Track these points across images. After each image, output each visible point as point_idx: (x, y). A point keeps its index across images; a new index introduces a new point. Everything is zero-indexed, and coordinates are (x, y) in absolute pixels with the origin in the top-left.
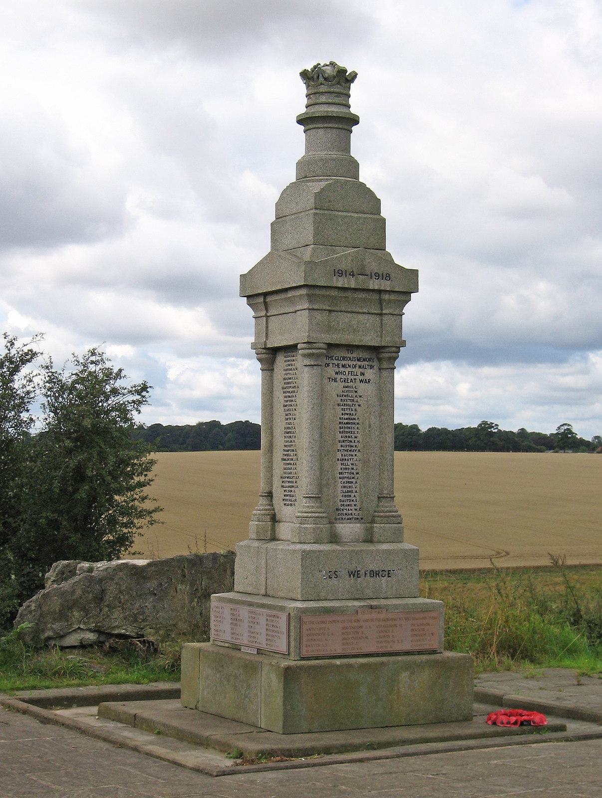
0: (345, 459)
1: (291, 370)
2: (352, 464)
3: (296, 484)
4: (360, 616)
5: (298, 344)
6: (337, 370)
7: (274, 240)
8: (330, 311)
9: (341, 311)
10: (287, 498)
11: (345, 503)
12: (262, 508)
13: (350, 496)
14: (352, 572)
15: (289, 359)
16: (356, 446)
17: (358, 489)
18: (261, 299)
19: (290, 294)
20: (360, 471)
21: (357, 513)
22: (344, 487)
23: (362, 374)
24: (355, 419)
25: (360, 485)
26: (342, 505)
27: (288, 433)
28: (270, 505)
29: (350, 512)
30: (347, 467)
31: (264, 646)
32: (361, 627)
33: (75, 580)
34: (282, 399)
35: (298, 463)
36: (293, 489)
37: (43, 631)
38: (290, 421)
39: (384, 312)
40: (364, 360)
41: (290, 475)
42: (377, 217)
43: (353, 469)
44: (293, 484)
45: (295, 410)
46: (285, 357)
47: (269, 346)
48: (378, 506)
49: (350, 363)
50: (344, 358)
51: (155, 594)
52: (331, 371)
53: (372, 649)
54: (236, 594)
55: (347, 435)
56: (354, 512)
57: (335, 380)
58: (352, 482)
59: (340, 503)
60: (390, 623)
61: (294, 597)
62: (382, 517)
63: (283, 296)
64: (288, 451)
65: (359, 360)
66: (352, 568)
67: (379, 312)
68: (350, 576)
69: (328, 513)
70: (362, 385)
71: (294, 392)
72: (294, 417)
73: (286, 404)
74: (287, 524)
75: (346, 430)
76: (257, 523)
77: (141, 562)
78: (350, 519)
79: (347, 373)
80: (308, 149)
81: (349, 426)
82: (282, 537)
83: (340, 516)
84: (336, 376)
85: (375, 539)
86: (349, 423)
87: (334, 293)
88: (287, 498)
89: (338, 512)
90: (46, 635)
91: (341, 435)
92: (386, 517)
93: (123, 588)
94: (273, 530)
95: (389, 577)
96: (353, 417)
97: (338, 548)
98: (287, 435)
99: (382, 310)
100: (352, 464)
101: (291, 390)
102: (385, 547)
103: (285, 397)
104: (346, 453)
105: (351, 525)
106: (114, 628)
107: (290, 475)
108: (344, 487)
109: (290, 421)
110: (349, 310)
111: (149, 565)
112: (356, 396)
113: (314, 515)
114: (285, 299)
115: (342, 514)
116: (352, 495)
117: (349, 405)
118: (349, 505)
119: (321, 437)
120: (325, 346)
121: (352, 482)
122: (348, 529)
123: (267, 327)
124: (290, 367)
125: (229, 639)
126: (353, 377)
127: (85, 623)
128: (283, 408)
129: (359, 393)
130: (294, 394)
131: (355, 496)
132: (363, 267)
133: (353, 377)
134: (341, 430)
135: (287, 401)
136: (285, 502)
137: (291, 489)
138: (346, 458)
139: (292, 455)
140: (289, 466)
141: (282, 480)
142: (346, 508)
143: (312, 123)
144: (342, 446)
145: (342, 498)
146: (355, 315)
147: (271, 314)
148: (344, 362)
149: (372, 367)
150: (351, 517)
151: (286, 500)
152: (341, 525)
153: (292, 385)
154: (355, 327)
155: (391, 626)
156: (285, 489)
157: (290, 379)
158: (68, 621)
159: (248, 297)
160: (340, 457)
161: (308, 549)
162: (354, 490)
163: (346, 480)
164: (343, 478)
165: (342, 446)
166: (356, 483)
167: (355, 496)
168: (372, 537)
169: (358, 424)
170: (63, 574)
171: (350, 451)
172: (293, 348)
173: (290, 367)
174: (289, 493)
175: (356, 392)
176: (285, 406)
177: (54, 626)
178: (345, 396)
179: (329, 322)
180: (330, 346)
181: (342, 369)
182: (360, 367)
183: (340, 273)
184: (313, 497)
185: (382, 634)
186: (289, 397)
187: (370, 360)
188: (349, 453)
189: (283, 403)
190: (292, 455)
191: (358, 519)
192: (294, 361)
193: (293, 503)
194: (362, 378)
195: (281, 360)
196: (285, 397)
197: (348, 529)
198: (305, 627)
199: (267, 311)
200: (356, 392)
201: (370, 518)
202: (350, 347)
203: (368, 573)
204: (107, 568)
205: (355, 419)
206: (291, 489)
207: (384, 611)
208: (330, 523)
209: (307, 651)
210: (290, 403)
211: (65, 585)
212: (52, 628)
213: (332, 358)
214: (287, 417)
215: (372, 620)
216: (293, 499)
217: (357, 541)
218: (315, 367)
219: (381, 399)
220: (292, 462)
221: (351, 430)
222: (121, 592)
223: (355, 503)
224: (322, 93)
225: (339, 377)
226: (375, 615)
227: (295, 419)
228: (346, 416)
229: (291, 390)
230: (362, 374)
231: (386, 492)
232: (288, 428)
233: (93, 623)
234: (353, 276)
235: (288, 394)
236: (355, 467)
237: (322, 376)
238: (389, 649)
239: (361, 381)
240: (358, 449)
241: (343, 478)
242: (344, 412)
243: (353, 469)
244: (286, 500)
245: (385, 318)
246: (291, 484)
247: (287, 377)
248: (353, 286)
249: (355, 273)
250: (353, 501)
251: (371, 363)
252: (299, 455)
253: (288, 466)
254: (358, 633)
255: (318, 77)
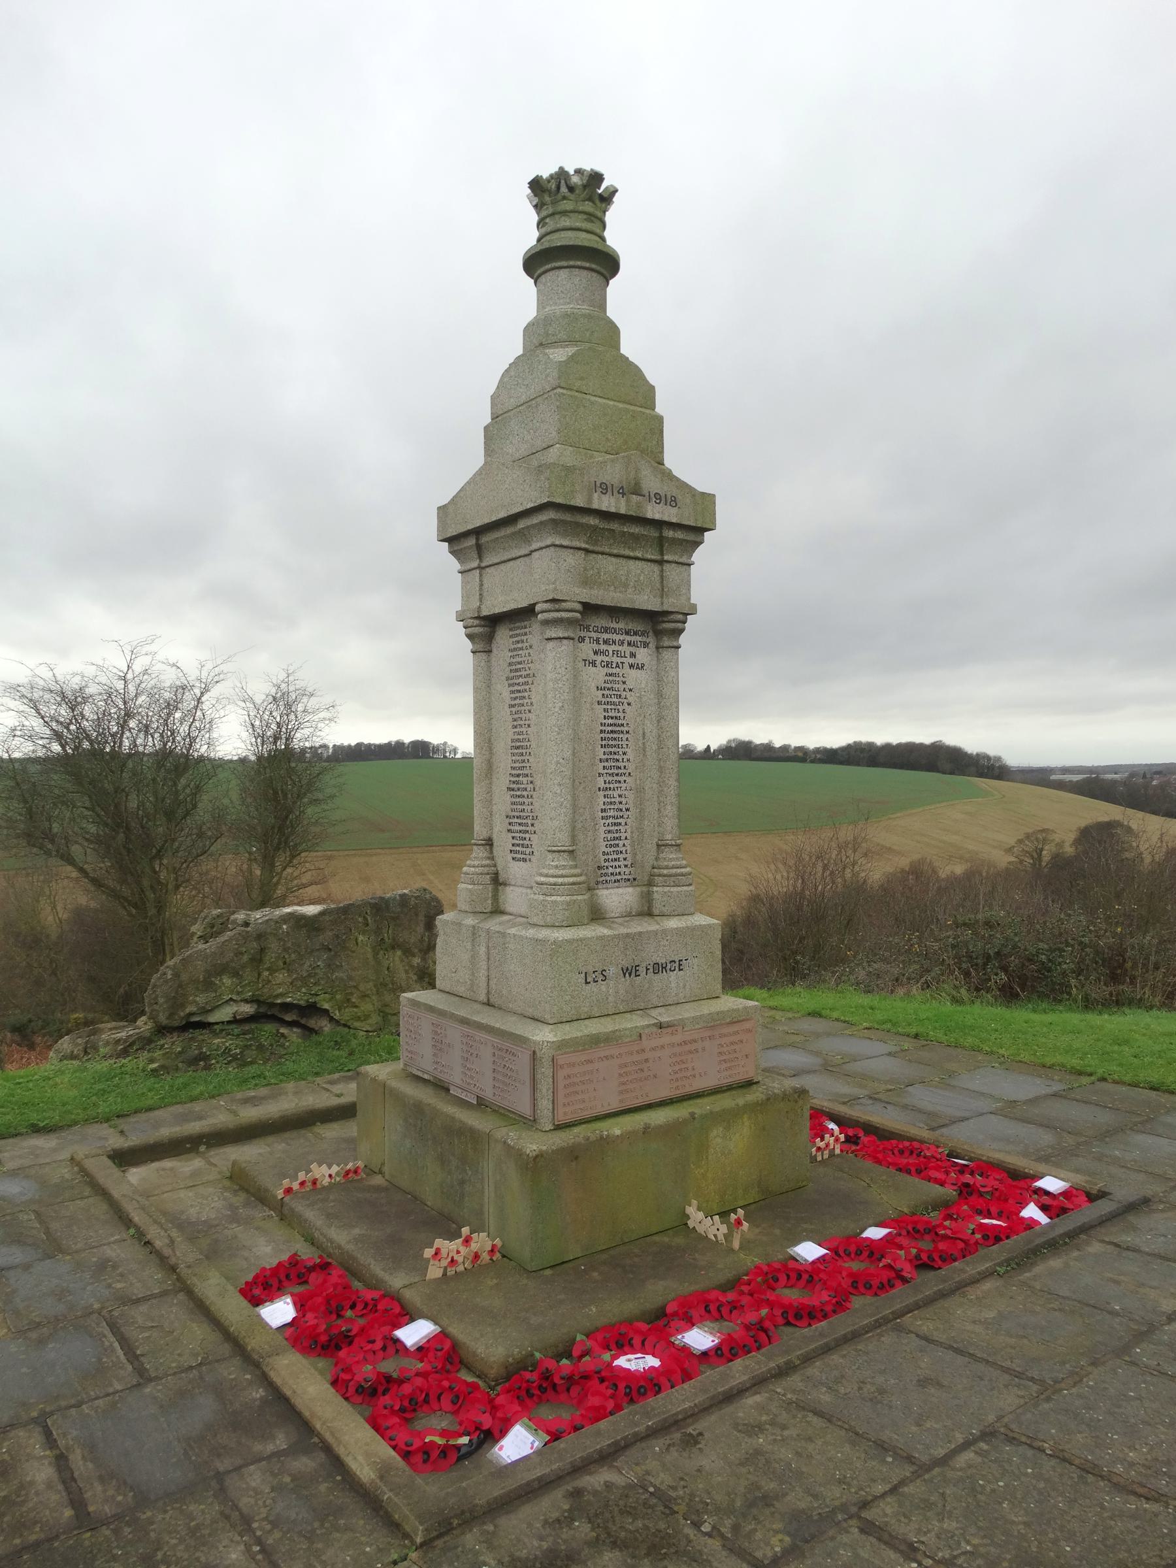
0: (610, 789)
1: (521, 649)
2: (620, 796)
3: (533, 829)
4: (646, 1043)
5: (535, 604)
6: (596, 647)
7: (489, 450)
8: (587, 551)
9: (603, 553)
10: (518, 848)
11: (610, 857)
12: (476, 863)
13: (618, 845)
14: (627, 969)
15: (518, 632)
16: (625, 767)
17: (628, 835)
18: (471, 541)
19: (522, 524)
20: (630, 806)
21: (627, 870)
22: (609, 832)
23: (633, 655)
24: (623, 725)
25: (632, 827)
26: (606, 860)
27: (518, 748)
28: (489, 858)
29: (618, 870)
30: (613, 800)
31: (488, 1094)
32: (647, 1060)
33: (226, 938)
34: (506, 694)
35: (534, 794)
36: (527, 836)
37: (183, 1006)
38: (522, 730)
39: (666, 558)
40: (636, 634)
41: (521, 814)
42: (651, 412)
43: (621, 803)
44: (527, 829)
45: (530, 711)
46: (511, 630)
47: (485, 612)
48: (657, 859)
49: (617, 637)
50: (606, 630)
51: (330, 950)
52: (587, 649)
53: (664, 1093)
54: (441, 996)
55: (613, 750)
56: (623, 869)
57: (593, 664)
58: (620, 824)
59: (603, 858)
60: (687, 1048)
61: (537, 1015)
62: (665, 876)
63: (509, 530)
64: (518, 776)
65: (627, 633)
66: (626, 963)
67: (658, 557)
68: (625, 975)
69: (586, 875)
70: (633, 672)
71: (526, 683)
72: (527, 722)
73: (513, 703)
74: (516, 889)
75: (611, 742)
76: (470, 887)
77: (311, 910)
78: (618, 881)
79: (611, 652)
80: (541, 304)
81: (615, 736)
82: (509, 909)
83: (604, 878)
84: (595, 657)
85: (656, 912)
86: (615, 732)
87: (593, 521)
88: (518, 848)
89: (599, 872)
90: (188, 1011)
91: (603, 750)
92: (670, 876)
93: (289, 945)
94: (495, 898)
95: (680, 970)
96: (620, 722)
97: (606, 932)
98: (516, 751)
99: (662, 554)
100: (620, 796)
101: (521, 680)
102: (673, 923)
103: (512, 692)
104: (610, 778)
105: (620, 891)
106: (277, 996)
107: (521, 814)
108: (609, 832)
109: (522, 730)
110: (615, 551)
111: (322, 913)
112: (624, 690)
113: (566, 880)
114: (513, 534)
115: (606, 875)
116: (621, 843)
117: (614, 703)
118: (615, 860)
119: (574, 754)
120: (579, 607)
121: (620, 824)
122: (616, 898)
123: (481, 585)
124: (520, 645)
125: (430, 1068)
126: (619, 660)
127: (238, 993)
128: (508, 711)
129: (629, 685)
130: (527, 687)
131: (624, 845)
132: (637, 484)
133: (619, 660)
134: (604, 743)
135: (515, 699)
136: (515, 855)
137: (524, 835)
138: (612, 786)
139: (525, 782)
140: (521, 800)
141: (508, 820)
142: (611, 864)
143: (548, 261)
144: (604, 768)
145: (607, 850)
146: (623, 561)
147: (488, 564)
148: (606, 636)
149: (646, 645)
150: (619, 877)
151: (517, 852)
152: (605, 892)
153: (523, 673)
154: (623, 578)
155: (690, 1052)
156: (513, 835)
157: (520, 663)
158: (216, 992)
159: (450, 540)
160: (602, 785)
161: (561, 939)
162: (623, 836)
163: (611, 820)
164: (607, 818)
165: (604, 768)
166: (626, 824)
167: (624, 845)
168: (650, 908)
169: (628, 732)
170: (212, 927)
171: (617, 775)
172: (528, 612)
173: (520, 645)
174: (521, 842)
175: (624, 683)
176: (512, 706)
177: (198, 999)
178: (609, 689)
179: (585, 569)
180: (589, 609)
181: (603, 647)
182: (629, 644)
183: (605, 489)
184: (564, 851)
185: (677, 1068)
186: (519, 691)
187: (643, 635)
188: (616, 778)
189: (509, 701)
190: (525, 782)
191: (629, 880)
192: (526, 634)
193: (528, 857)
194: (632, 661)
195: (503, 637)
196: (512, 692)
197: (616, 898)
198: (561, 1074)
199: (480, 558)
200: (624, 683)
201: (646, 878)
202: (615, 612)
203: (650, 967)
204: (267, 921)
205: (623, 725)
206: (524, 835)
207: (680, 1029)
208: (589, 889)
209: (565, 1113)
210: (521, 702)
211: (213, 944)
212: (195, 1002)
213: (587, 628)
214: (515, 723)
215: (663, 1047)
216: (528, 851)
217: (629, 915)
218: (565, 642)
219: (660, 695)
220: (525, 793)
221: (617, 743)
222: (286, 950)
223: (624, 856)
224: (564, 213)
225: (599, 658)
226: (666, 1039)
227: (529, 726)
228: (610, 721)
229: (521, 680)
230: (633, 655)
231: (669, 837)
232: (518, 740)
233: (249, 991)
234: (623, 494)
235: (516, 688)
236: (623, 800)
237: (575, 657)
238: (688, 1090)
239: (631, 666)
240: (627, 772)
241: (607, 818)
242: (606, 714)
243: (621, 803)
244: (517, 852)
245: (666, 567)
246: (524, 828)
247: (514, 660)
248: (623, 511)
249: (626, 490)
250: (621, 852)
251: (644, 639)
252: (538, 783)
253: (518, 800)
254: (642, 1070)
255: (558, 188)
